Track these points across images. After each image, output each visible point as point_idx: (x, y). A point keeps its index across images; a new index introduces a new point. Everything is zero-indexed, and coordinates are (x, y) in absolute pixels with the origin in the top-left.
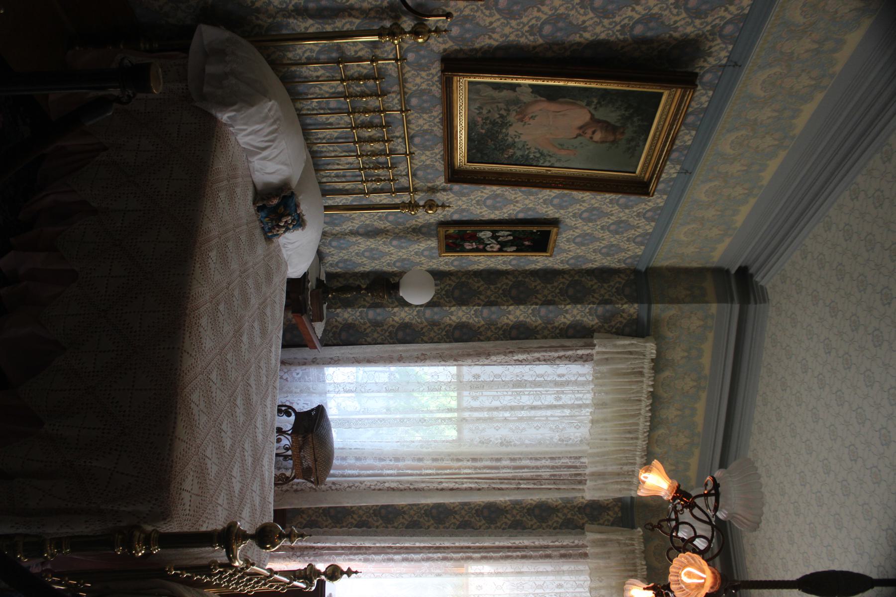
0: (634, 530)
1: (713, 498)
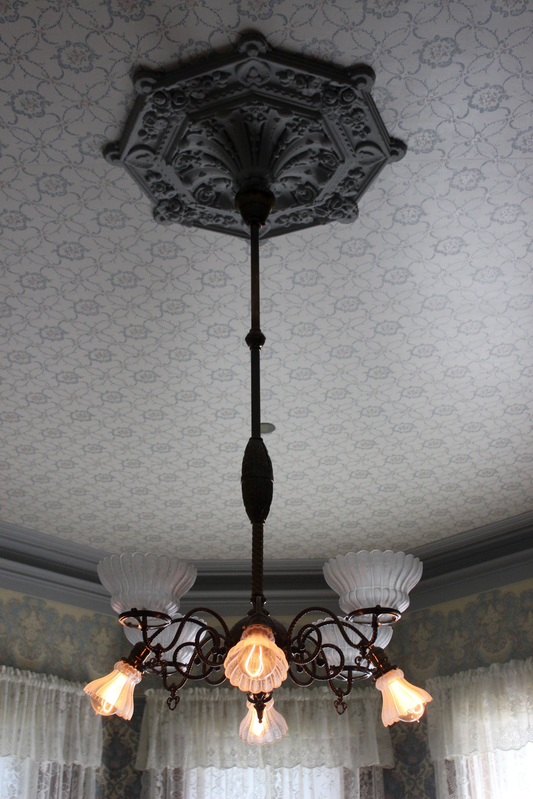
0: (147, 700)
1: (148, 618)
